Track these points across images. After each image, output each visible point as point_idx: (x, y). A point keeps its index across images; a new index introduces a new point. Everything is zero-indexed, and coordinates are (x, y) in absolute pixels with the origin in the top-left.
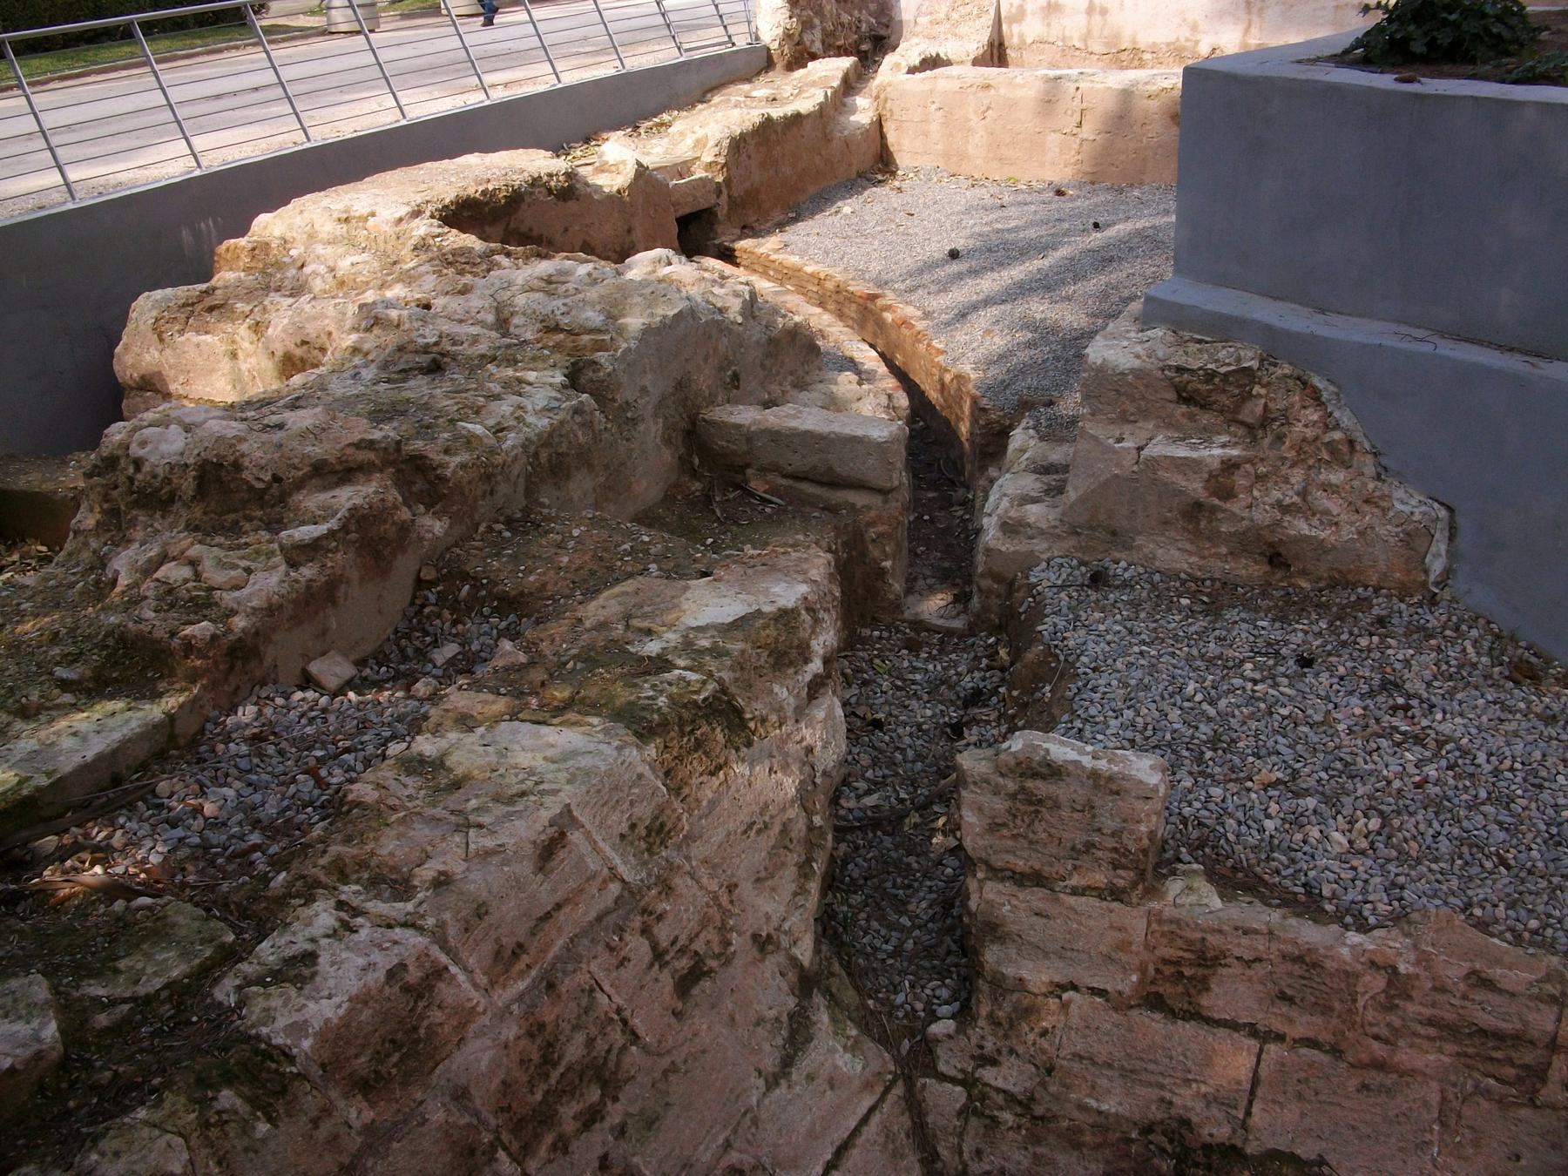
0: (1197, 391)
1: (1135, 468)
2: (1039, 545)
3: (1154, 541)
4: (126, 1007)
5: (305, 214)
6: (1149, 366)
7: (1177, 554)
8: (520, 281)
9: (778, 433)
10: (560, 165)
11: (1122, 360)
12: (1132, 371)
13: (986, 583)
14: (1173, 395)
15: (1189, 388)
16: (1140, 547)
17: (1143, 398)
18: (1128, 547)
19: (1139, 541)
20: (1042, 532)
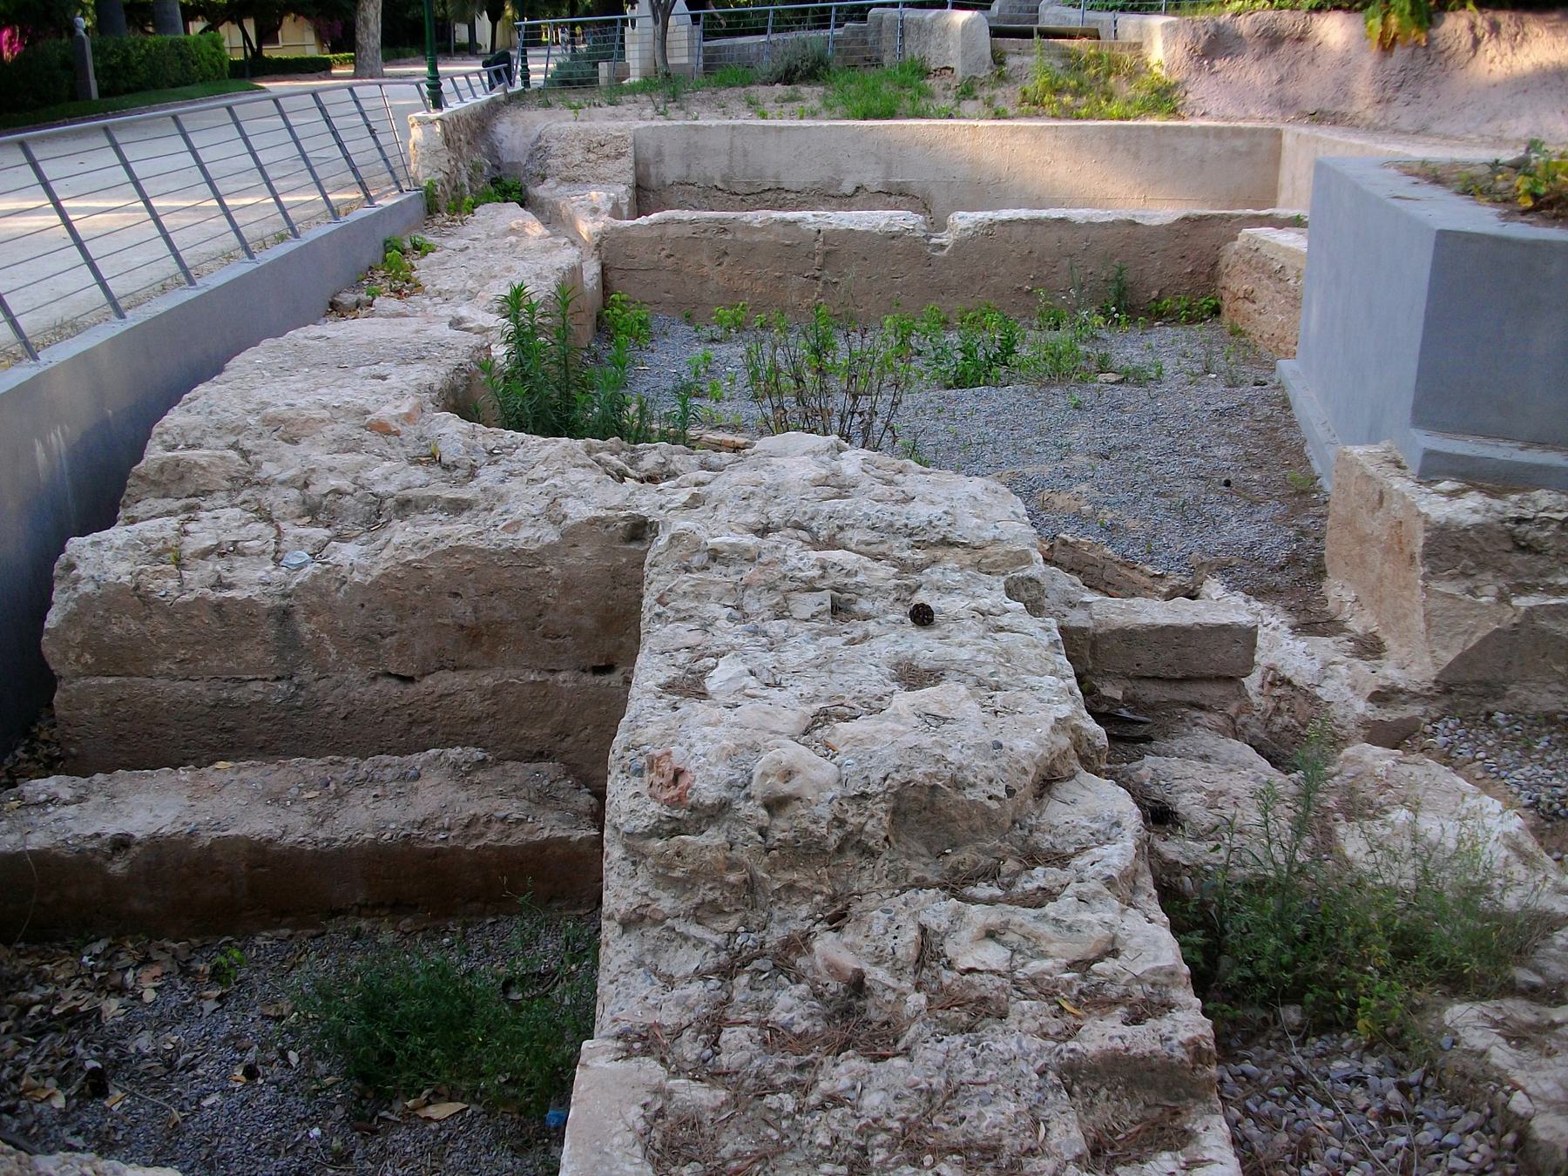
0: (1535, 539)
1: (1516, 620)
2: (1415, 710)
3: (1525, 687)
4: (261, 696)
5: (418, 433)
6: (1490, 521)
7: (1550, 696)
8: (975, 1106)
9: (1133, 632)
10: (602, 82)
11: (1462, 517)
12: (1475, 526)
13: (1471, 802)
14: (1508, 546)
15: (1529, 537)
16: (1514, 696)
17: (1483, 551)
18: (1497, 697)
19: (1513, 689)
20: (1415, 696)
